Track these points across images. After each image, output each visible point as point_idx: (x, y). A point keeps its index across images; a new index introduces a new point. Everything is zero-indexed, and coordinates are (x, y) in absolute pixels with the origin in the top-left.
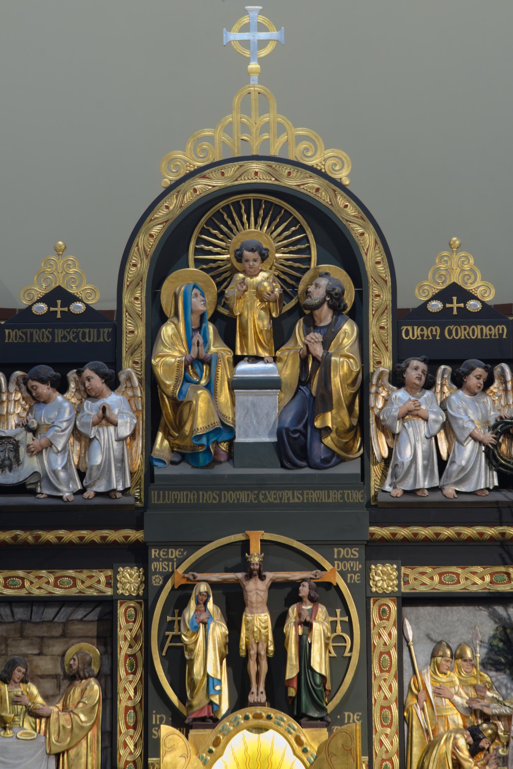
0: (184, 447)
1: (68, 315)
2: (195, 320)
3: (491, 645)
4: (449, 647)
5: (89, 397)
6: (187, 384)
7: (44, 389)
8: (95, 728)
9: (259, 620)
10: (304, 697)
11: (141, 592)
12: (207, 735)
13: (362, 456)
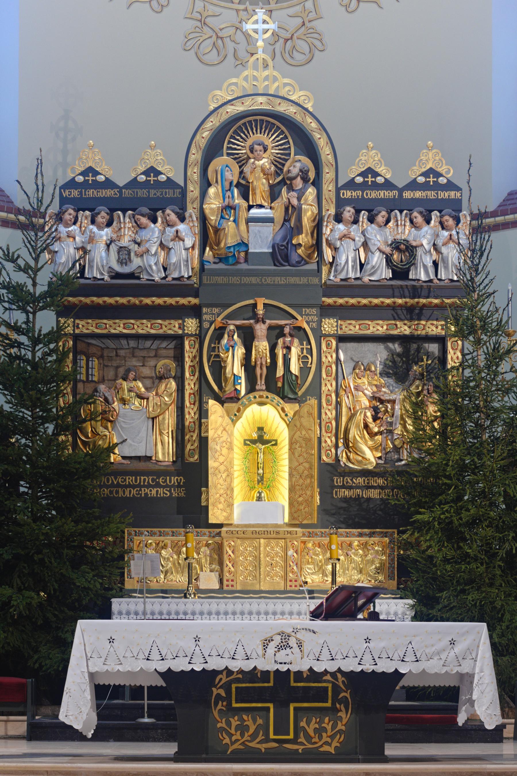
0: (221, 254)
1: (157, 182)
2: (227, 185)
3: (385, 364)
4: (362, 364)
5: (169, 225)
6: (222, 220)
7: (144, 220)
8: (173, 405)
9: (262, 346)
10: (286, 387)
11: (197, 332)
12: (233, 406)
13: (318, 262)
